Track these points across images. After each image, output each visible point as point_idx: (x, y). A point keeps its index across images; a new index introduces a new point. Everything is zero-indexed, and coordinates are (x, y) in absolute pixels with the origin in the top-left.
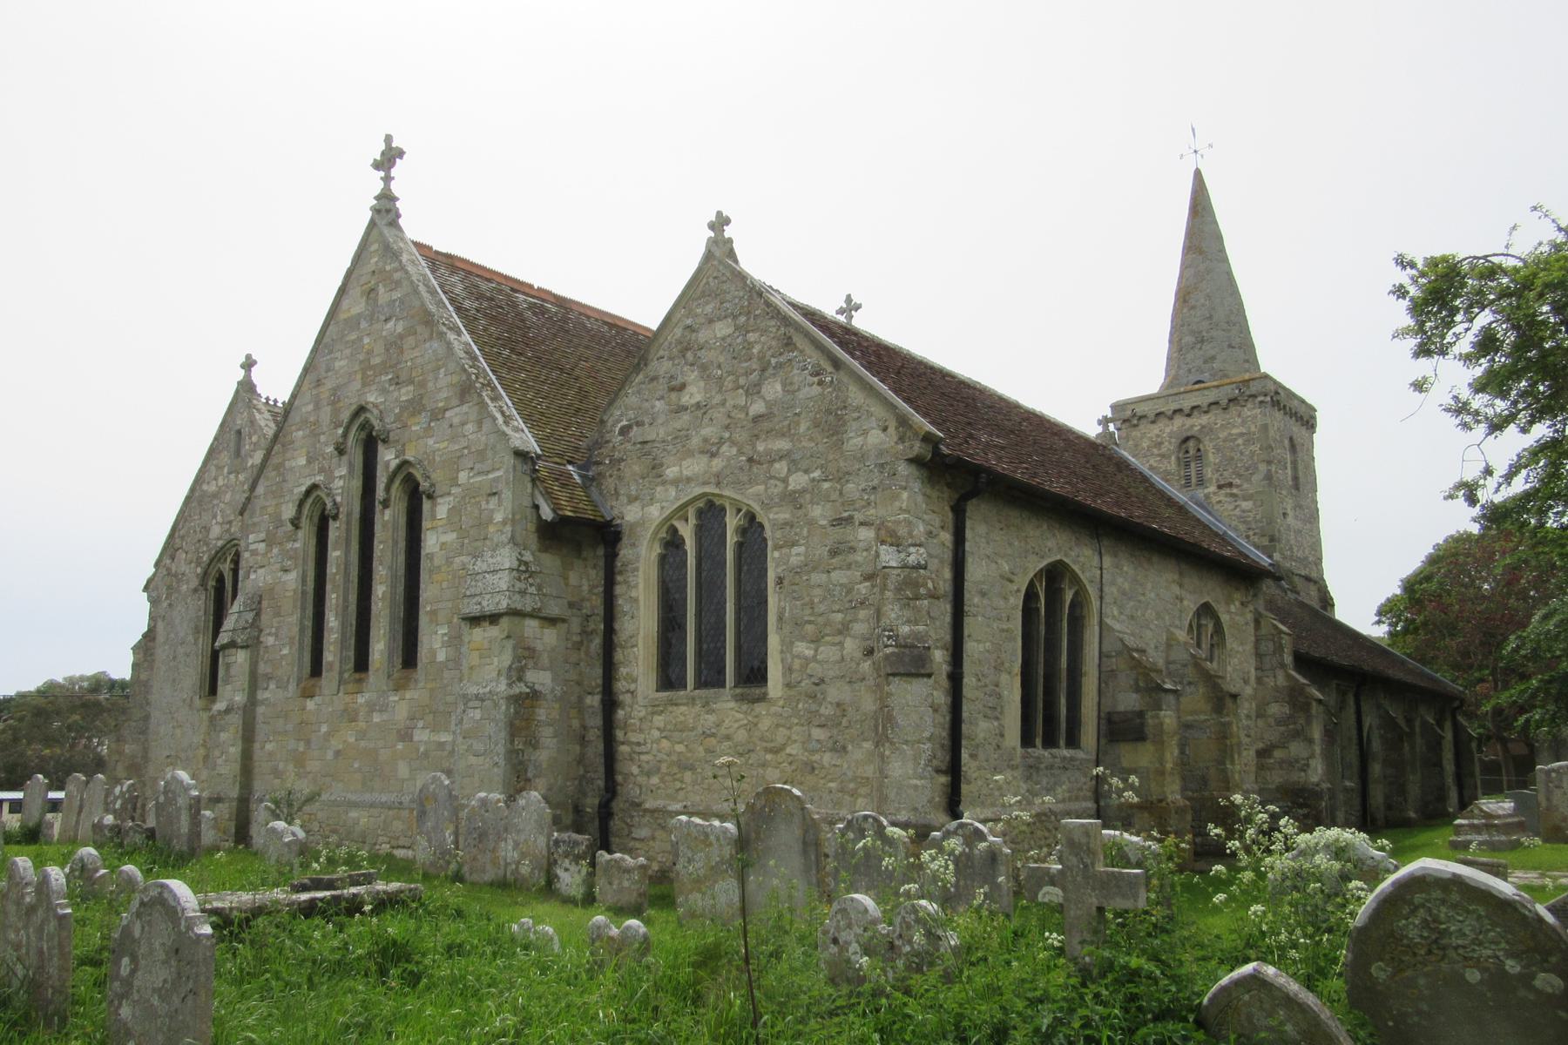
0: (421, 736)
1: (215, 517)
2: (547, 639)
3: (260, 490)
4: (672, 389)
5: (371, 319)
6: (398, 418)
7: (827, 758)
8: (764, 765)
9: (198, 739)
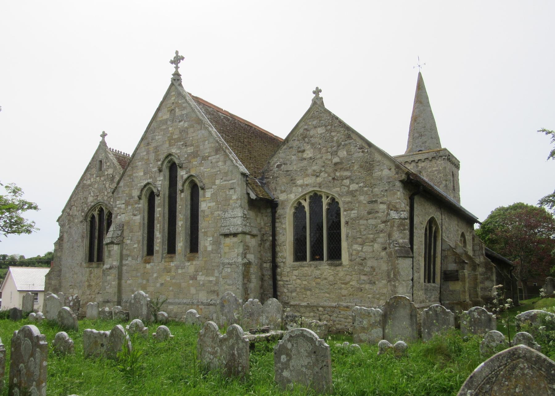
0: (201, 278)
1: (90, 193)
3: (121, 184)
4: (299, 152)
5: (173, 121)
6: (186, 159)
7: (367, 286)
8: (341, 289)
9: (85, 279)
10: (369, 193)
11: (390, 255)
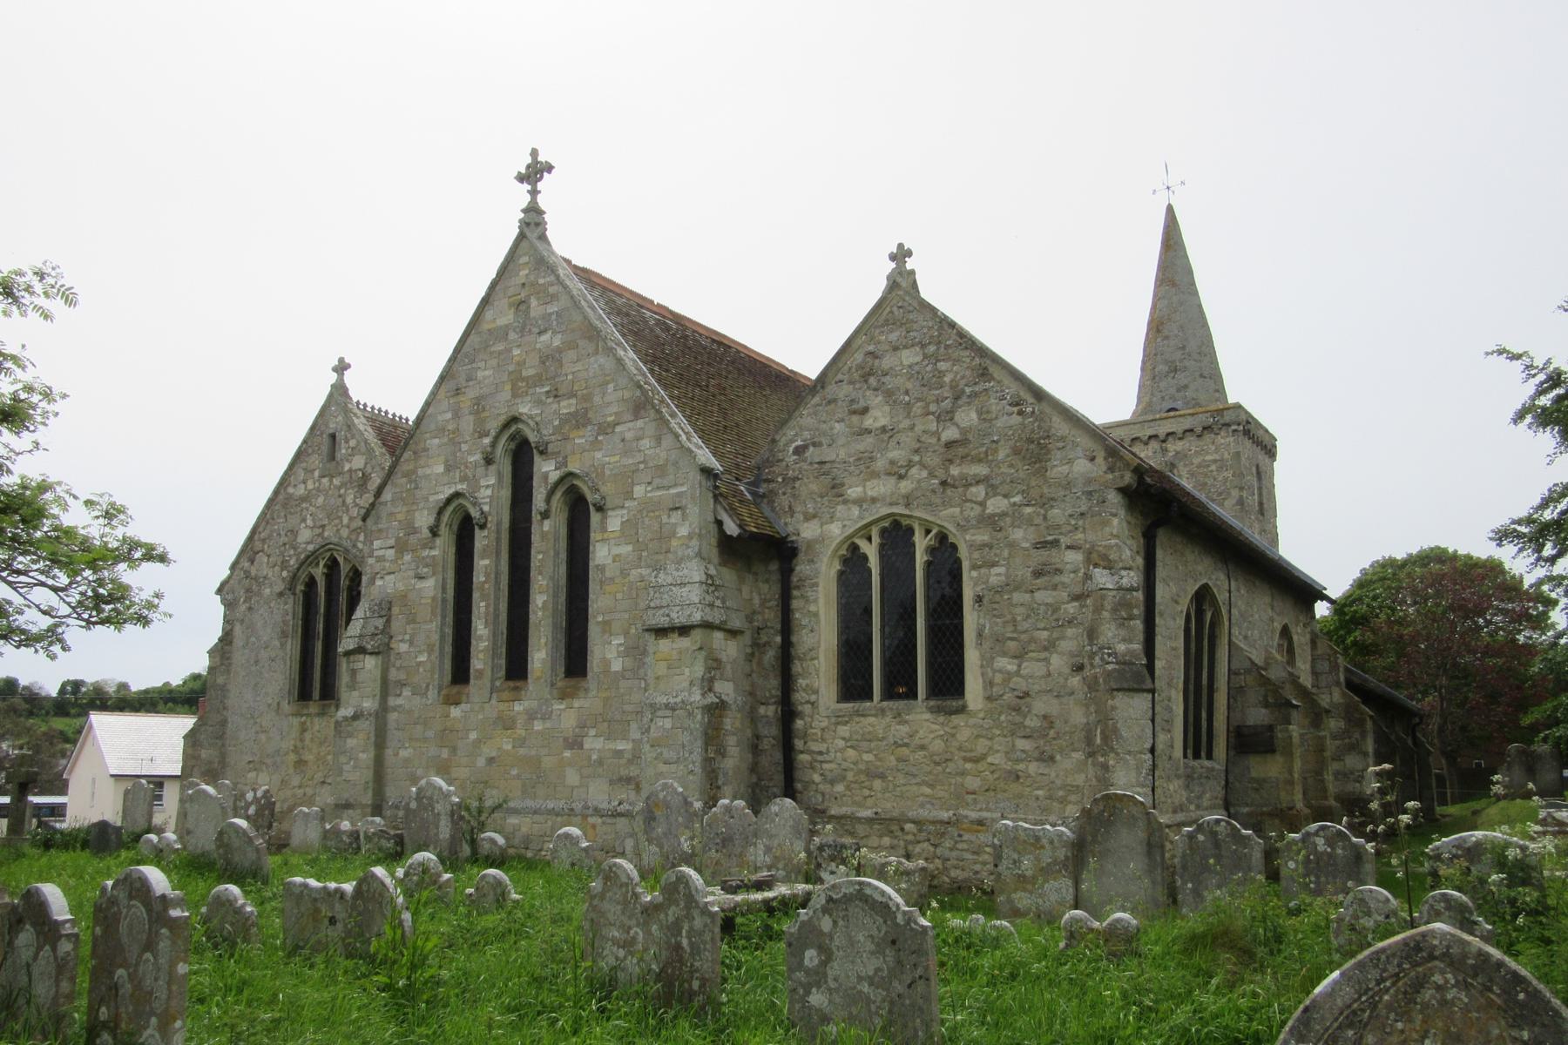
1: (304, 520)
2: (730, 650)
3: (387, 495)
4: (854, 412)
5: (522, 331)
6: (557, 430)
7: (1033, 768)
8: (963, 773)
9: (288, 744)
10: (1038, 520)
11: (1092, 685)
